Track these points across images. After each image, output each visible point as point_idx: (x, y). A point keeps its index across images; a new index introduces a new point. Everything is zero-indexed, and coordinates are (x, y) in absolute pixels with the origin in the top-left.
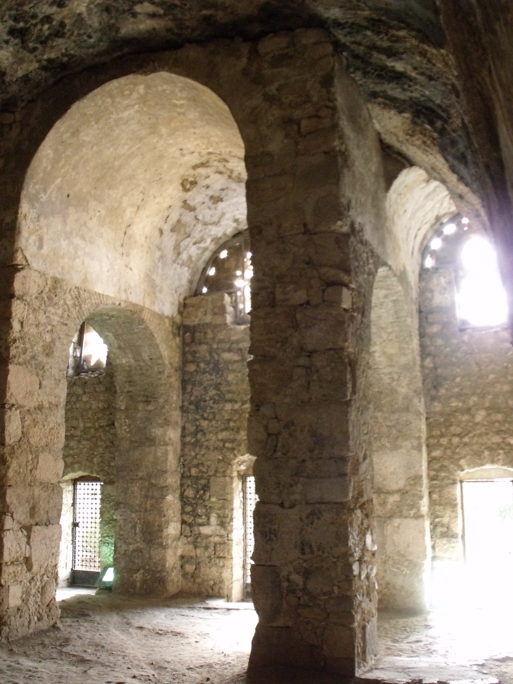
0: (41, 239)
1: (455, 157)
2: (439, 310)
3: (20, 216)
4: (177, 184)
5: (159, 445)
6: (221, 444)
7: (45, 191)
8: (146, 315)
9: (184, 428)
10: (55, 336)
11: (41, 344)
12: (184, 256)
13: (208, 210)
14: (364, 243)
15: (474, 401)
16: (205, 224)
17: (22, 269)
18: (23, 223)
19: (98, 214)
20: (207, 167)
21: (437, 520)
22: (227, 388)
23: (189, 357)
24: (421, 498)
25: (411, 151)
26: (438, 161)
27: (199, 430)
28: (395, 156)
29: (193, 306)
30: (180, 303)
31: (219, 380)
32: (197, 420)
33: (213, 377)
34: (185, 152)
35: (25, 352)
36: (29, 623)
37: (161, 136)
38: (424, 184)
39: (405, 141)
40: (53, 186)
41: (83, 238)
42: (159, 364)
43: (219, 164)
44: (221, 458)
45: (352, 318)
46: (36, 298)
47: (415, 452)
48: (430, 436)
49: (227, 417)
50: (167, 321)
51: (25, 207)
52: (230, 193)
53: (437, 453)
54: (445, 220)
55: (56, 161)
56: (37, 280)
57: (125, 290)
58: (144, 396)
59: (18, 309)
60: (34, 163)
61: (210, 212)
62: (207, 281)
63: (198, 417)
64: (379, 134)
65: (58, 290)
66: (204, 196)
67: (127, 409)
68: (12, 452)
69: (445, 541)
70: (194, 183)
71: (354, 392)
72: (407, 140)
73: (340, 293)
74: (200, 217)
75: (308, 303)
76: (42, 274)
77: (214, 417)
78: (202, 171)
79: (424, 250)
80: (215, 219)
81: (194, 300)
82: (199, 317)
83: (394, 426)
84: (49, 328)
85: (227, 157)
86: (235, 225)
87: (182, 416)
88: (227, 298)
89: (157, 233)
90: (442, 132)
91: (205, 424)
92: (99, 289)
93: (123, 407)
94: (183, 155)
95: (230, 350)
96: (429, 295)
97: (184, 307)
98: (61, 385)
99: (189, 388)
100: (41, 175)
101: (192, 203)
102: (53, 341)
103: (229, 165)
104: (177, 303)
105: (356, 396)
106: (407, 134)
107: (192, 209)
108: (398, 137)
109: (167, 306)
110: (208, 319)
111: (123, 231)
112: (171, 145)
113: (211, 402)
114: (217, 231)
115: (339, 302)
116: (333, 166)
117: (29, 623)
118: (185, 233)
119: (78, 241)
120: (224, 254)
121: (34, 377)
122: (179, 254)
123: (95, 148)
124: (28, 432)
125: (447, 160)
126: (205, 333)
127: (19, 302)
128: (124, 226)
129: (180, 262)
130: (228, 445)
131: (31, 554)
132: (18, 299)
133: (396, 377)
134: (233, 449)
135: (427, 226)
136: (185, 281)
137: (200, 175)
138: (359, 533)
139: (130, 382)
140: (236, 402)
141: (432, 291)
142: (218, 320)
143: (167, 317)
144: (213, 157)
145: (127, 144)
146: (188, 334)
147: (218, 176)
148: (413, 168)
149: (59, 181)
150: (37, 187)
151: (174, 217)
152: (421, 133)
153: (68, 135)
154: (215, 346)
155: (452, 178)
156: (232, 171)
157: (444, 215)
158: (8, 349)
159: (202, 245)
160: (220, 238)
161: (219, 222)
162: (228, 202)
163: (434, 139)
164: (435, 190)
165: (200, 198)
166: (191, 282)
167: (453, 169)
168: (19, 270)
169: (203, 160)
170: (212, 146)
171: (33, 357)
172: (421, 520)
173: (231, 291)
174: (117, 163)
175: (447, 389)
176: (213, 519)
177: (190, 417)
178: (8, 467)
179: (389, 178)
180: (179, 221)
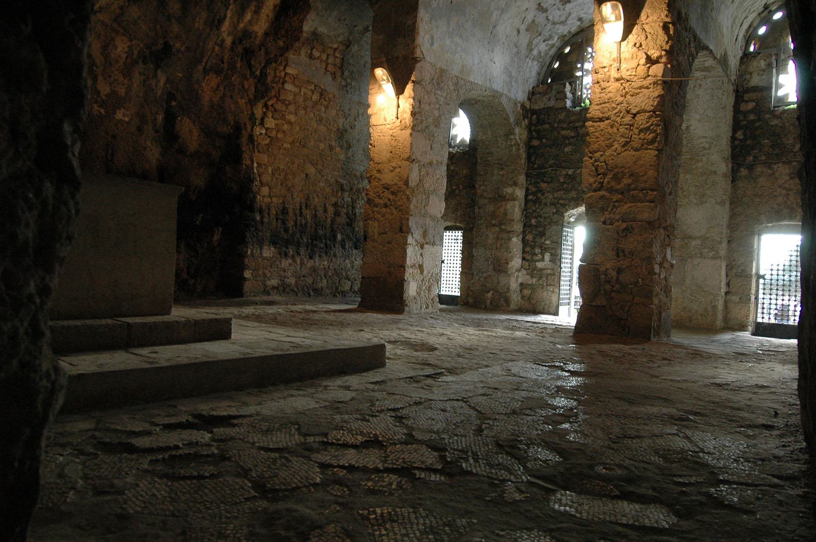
0: (432, 38)
3: (419, 19)
8: (504, 101)
9: (527, 189)
12: (535, 52)
13: (557, 11)
16: (554, 23)
23: (534, 134)
42: (511, 139)
61: (559, 13)
62: (551, 72)
63: (539, 181)
74: (550, 18)
76: (433, 65)
80: (563, 18)
86: (579, 23)
87: (527, 180)
89: (515, 33)
92: (471, 79)
101: (545, 6)
102: (440, 116)
110: (552, 103)
114: (563, 30)
120: (567, 50)
122: (531, 50)
136: (534, 74)
141: (751, 74)
142: (559, 105)
143: (520, 102)
159: (550, 42)
160: (565, 36)
161: (566, 21)
166: (539, 74)
173: (572, 80)
176: (547, 256)
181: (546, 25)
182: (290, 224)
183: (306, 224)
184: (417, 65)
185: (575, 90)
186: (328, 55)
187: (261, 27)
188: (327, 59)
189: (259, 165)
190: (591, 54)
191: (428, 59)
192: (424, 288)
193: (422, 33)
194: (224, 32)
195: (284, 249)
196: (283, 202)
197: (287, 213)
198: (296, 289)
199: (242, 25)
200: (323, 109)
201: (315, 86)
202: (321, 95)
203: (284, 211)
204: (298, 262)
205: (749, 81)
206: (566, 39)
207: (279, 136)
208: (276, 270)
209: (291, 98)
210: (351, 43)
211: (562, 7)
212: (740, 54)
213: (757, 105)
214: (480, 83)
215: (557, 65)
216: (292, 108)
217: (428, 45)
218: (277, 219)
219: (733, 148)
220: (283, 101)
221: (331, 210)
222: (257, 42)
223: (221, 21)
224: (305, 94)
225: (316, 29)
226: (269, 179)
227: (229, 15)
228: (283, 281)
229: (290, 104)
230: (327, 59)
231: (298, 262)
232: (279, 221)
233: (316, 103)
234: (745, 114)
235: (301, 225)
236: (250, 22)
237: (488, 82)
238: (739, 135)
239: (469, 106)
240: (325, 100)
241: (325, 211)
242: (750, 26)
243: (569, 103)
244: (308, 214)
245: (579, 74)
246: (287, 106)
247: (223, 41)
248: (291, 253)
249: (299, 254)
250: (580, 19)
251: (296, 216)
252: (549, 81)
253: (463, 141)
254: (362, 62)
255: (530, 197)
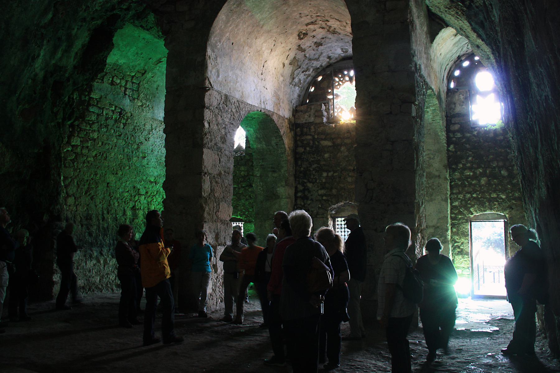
0: (218, 72)
1: (476, 23)
2: (459, 115)
3: (207, 57)
4: (295, 35)
5: (282, 198)
6: (320, 198)
7: (220, 42)
8: (275, 118)
9: (296, 188)
10: (227, 131)
11: (220, 136)
12: (296, 80)
13: (312, 51)
14: (421, 76)
15: (480, 172)
16: (310, 60)
17: (209, 90)
18: (209, 61)
19: (249, 55)
20: (316, 24)
21: (456, 244)
22: (324, 163)
23: (299, 143)
24: (447, 230)
25: (448, 18)
26: (466, 25)
27: (306, 189)
28: (437, 20)
29: (301, 111)
30: (293, 110)
31: (319, 158)
32: (306, 183)
33: (315, 156)
34: (303, 15)
35: (211, 141)
36: (217, 303)
37: (289, 6)
38: (453, 37)
39: (444, 12)
40: (224, 38)
41: (241, 70)
42: (282, 148)
43: (323, 23)
44: (320, 206)
45: (416, 121)
46: (217, 108)
47: (443, 203)
48: (452, 193)
49: (324, 181)
50: (286, 121)
51: (209, 51)
52: (327, 40)
53: (456, 204)
54: (463, 58)
55: (227, 22)
56: (217, 96)
57: (264, 102)
58: (272, 168)
59: (207, 114)
60: (215, 24)
61: (314, 52)
62: (307, 94)
63: (305, 181)
64: (428, 7)
65: (228, 103)
66: (311, 42)
67: (261, 176)
68: (206, 202)
69: (460, 257)
70: (306, 34)
71: (417, 166)
72: (446, 11)
73: (411, 106)
74: (307, 55)
75: (391, 113)
76: (219, 93)
77: (316, 181)
78: (311, 27)
79: (450, 77)
80: (317, 56)
81: (303, 108)
82: (304, 119)
83: (430, 187)
84: (224, 126)
85: (329, 19)
86: (328, 60)
87: (295, 180)
88: (323, 107)
89: (282, 66)
90: (469, 7)
91: (310, 185)
92: (250, 102)
93: (258, 175)
94: (301, 17)
95: (325, 139)
96: (453, 106)
97: (295, 111)
98: (230, 161)
99: (299, 162)
100: (218, 31)
101: (303, 47)
102: (226, 134)
103: (329, 24)
104: (292, 110)
105: (418, 168)
106: (446, 8)
107: (304, 51)
108: (440, 9)
109: (285, 112)
110: (312, 119)
111: (262, 65)
112: (295, 11)
113: (314, 172)
114: (316, 64)
115: (410, 113)
116: (405, 31)
117: (217, 303)
118: (298, 65)
119: (238, 72)
120: (320, 78)
121: (217, 156)
122: (294, 79)
123: (250, 14)
124: (214, 190)
125: (471, 25)
126: (310, 129)
127: (207, 110)
128: (263, 62)
129: (294, 84)
130: (324, 198)
131: (216, 263)
132: (207, 108)
133: (432, 157)
134: (328, 200)
135: (452, 62)
136: (296, 96)
137: (310, 29)
138: (420, 247)
139: (263, 159)
140: (330, 171)
141: (455, 104)
142: (318, 121)
143: (287, 118)
144: (319, 18)
145: (268, 11)
146: (299, 129)
147: (321, 30)
148: (448, 28)
149: (228, 34)
150: (216, 39)
151: (292, 56)
152: (456, 8)
153: (235, 6)
154: (316, 137)
155: (473, 36)
156: (330, 27)
157: (463, 55)
158: (202, 139)
159: (307, 73)
160: (319, 68)
161: (319, 58)
162: (325, 46)
163: (463, 11)
164: (459, 40)
165: (308, 44)
166: (299, 96)
167: (474, 30)
168: (207, 91)
169: (313, 20)
170: (320, 11)
171: (216, 144)
172: (447, 244)
173: (325, 102)
174: (262, 23)
175: (463, 165)
177: (301, 181)
178: (204, 211)
179: (432, 35)
180: (295, 58)
181: (304, 61)
182: (94, 229)
183: (108, 227)
184: (207, 93)
185: (329, 109)
186: (127, 81)
187: (71, 62)
188: (126, 84)
189: (65, 178)
190: (338, 82)
191: (215, 87)
192: (218, 284)
193: (210, 67)
194: (37, 68)
195: (89, 251)
196: (87, 209)
197: (91, 219)
198: (100, 286)
199: (53, 62)
200: (122, 126)
201: (116, 107)
202: (120, 113)
203: (88, 217)
204: (102, 262)
205: (454, 109)
206: (319, 70)
207: (84, 151)
208: (82, 271)
209: (94, 118)
210: (146, 71)
211: (316, 49)
212: (446, 90)
213: (461, 126)
214: (257, 105)
215: (312, 90)
216: (95, 127)
217: (215, 77)
218: (82, 226)
219: (449, 157)
220: (88, 123)
221: (129, 213)
222: (67, 75)
223: (34, 59)
224: (106, 114)
225: (117, 61)
226: (75, 190)
227: (42, 54)
228: (89, 280)
229: (93, 123)
230: (126, 84)
231: (102, 262)
232: (84, 226)
233: (116, 121)
234: (454, 132)
235: (103, 228)
236: (61, 59)
237: (262, 104)
238: (452, 147)
239: (247, 122)
240: (124, 119)
241: (124, 213)
242: (450, 71)
243: (325, 120)
244: (109, 218)
245: (330, 97)
246: (91, 125)
247: (36, 75)
248: (95, 254)
249: (102, 254)
250: (329, 57)
251: (98, 220)
252: (440, 329)
253: (239, 147)
254: (155, 86)
255: (299, 194)
